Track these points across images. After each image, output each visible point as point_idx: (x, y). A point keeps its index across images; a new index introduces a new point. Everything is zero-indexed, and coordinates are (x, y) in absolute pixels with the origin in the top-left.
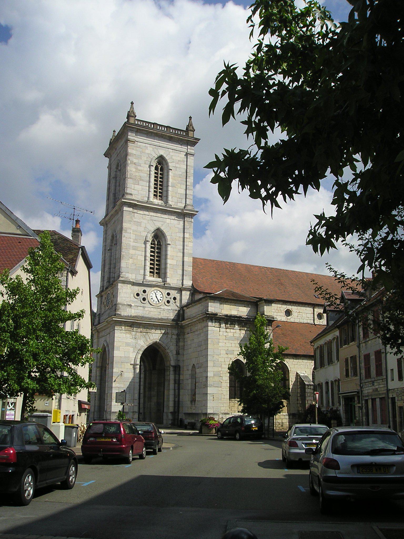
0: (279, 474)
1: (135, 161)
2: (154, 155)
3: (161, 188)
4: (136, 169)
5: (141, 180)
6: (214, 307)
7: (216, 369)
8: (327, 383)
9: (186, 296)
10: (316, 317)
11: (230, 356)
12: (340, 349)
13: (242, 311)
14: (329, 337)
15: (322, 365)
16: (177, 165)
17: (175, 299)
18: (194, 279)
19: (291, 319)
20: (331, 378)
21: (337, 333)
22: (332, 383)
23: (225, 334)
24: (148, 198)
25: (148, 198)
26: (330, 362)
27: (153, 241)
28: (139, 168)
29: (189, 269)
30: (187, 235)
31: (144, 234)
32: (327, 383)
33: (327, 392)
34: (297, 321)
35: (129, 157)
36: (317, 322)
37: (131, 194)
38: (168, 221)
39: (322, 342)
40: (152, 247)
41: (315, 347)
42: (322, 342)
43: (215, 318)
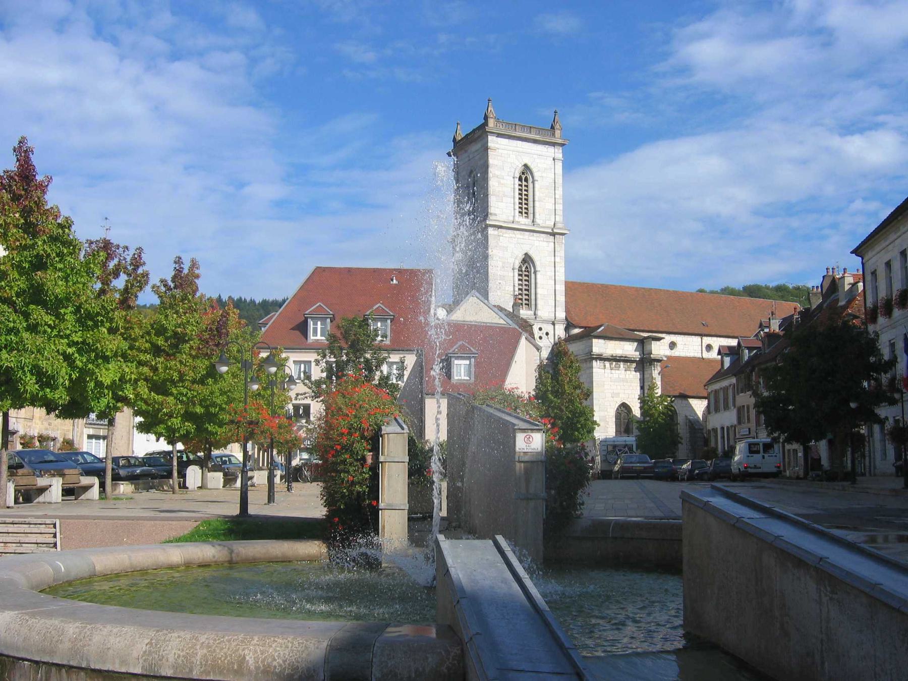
0: (207, 551)
1: (497, 173)
2: (518, 163)
3: (525, 204)
4: (499, 183)
5: (505, 196)
6: (599, 346)
7: (602, 414)
8: (723, 428)
9: (560, 332)
10: (704, 349)
11: (615, 399)
12: (737, 396)
13: (629, 349)
14: (725, 383)
15: (717, 410)
16: (544, 175)
17: (547, 334)
18: (567, 311)
19: (676, 353)
20: (727, 424)
21: (733, 380)
22: (728, 428)
23: (610, 375)
24: (514, 216)
25: (514, 216)
26: (726, 408)
27: (520, 267)
28: (502, 181)
29: (561, 298)
30: (557, 259)
31: (511, 261)
32: (723, 428)
33: (723, 437)
34: (683, 354)
35: (490, 169)
36: (706, 355)
37: (495, 215)
38: (537, 243)
39: (716, 386)
40: (519, 275)
41: (709, 390)
42: (716, 386)
43: (600, 358)
